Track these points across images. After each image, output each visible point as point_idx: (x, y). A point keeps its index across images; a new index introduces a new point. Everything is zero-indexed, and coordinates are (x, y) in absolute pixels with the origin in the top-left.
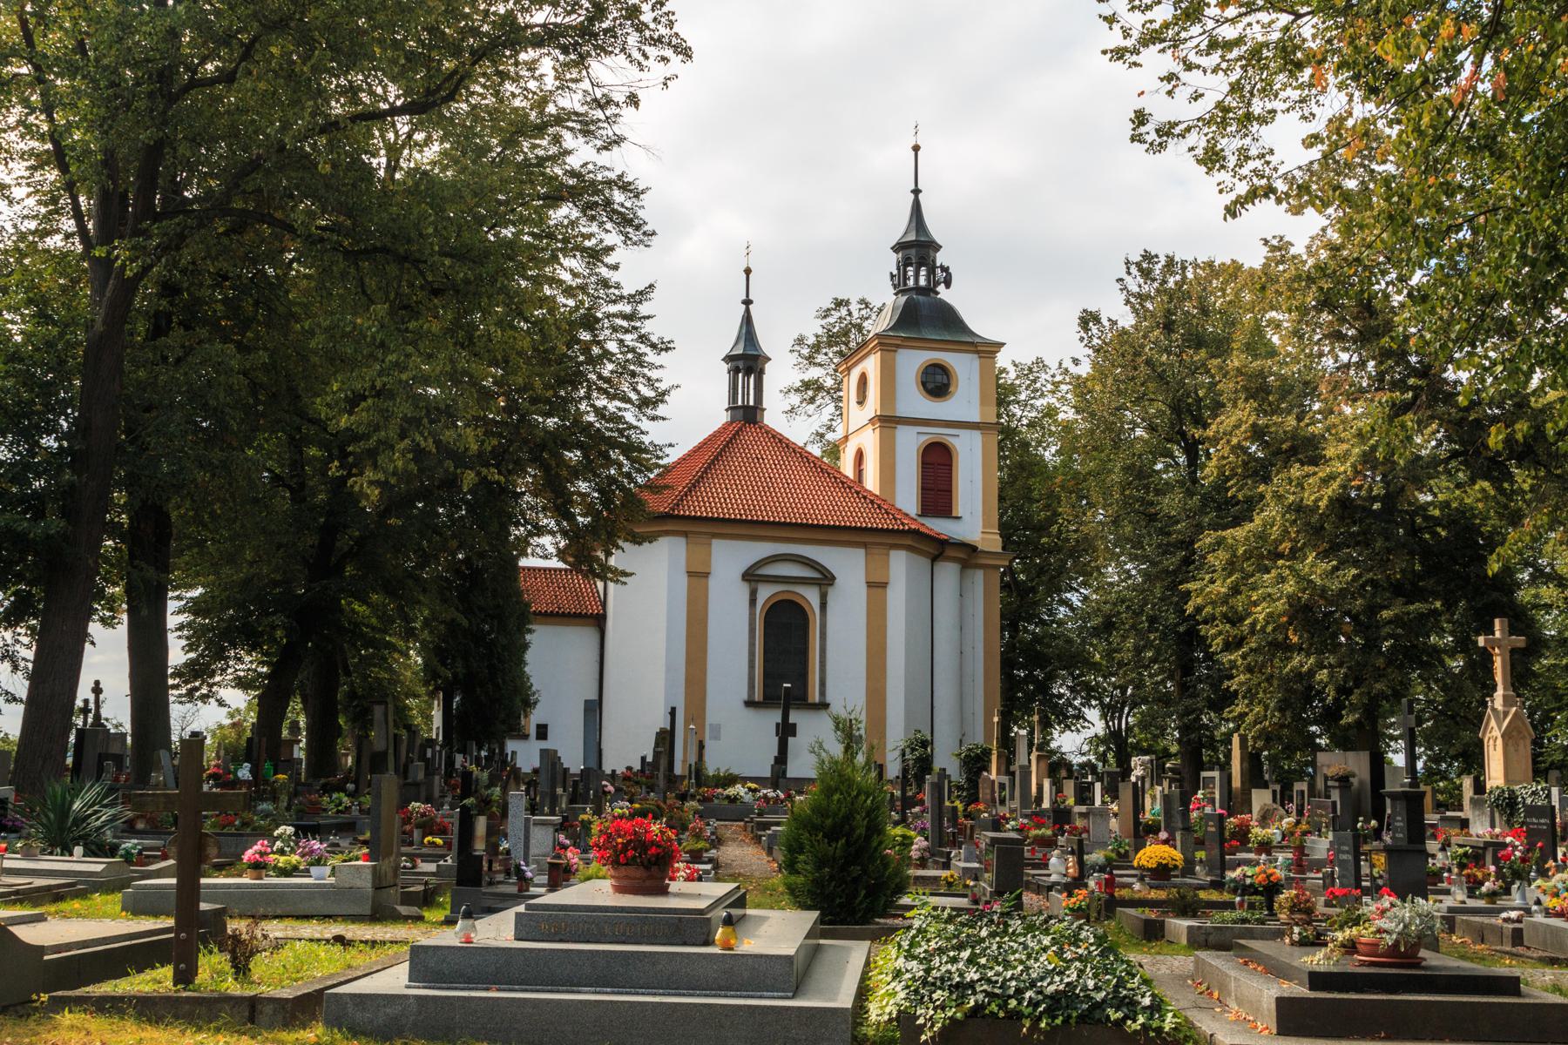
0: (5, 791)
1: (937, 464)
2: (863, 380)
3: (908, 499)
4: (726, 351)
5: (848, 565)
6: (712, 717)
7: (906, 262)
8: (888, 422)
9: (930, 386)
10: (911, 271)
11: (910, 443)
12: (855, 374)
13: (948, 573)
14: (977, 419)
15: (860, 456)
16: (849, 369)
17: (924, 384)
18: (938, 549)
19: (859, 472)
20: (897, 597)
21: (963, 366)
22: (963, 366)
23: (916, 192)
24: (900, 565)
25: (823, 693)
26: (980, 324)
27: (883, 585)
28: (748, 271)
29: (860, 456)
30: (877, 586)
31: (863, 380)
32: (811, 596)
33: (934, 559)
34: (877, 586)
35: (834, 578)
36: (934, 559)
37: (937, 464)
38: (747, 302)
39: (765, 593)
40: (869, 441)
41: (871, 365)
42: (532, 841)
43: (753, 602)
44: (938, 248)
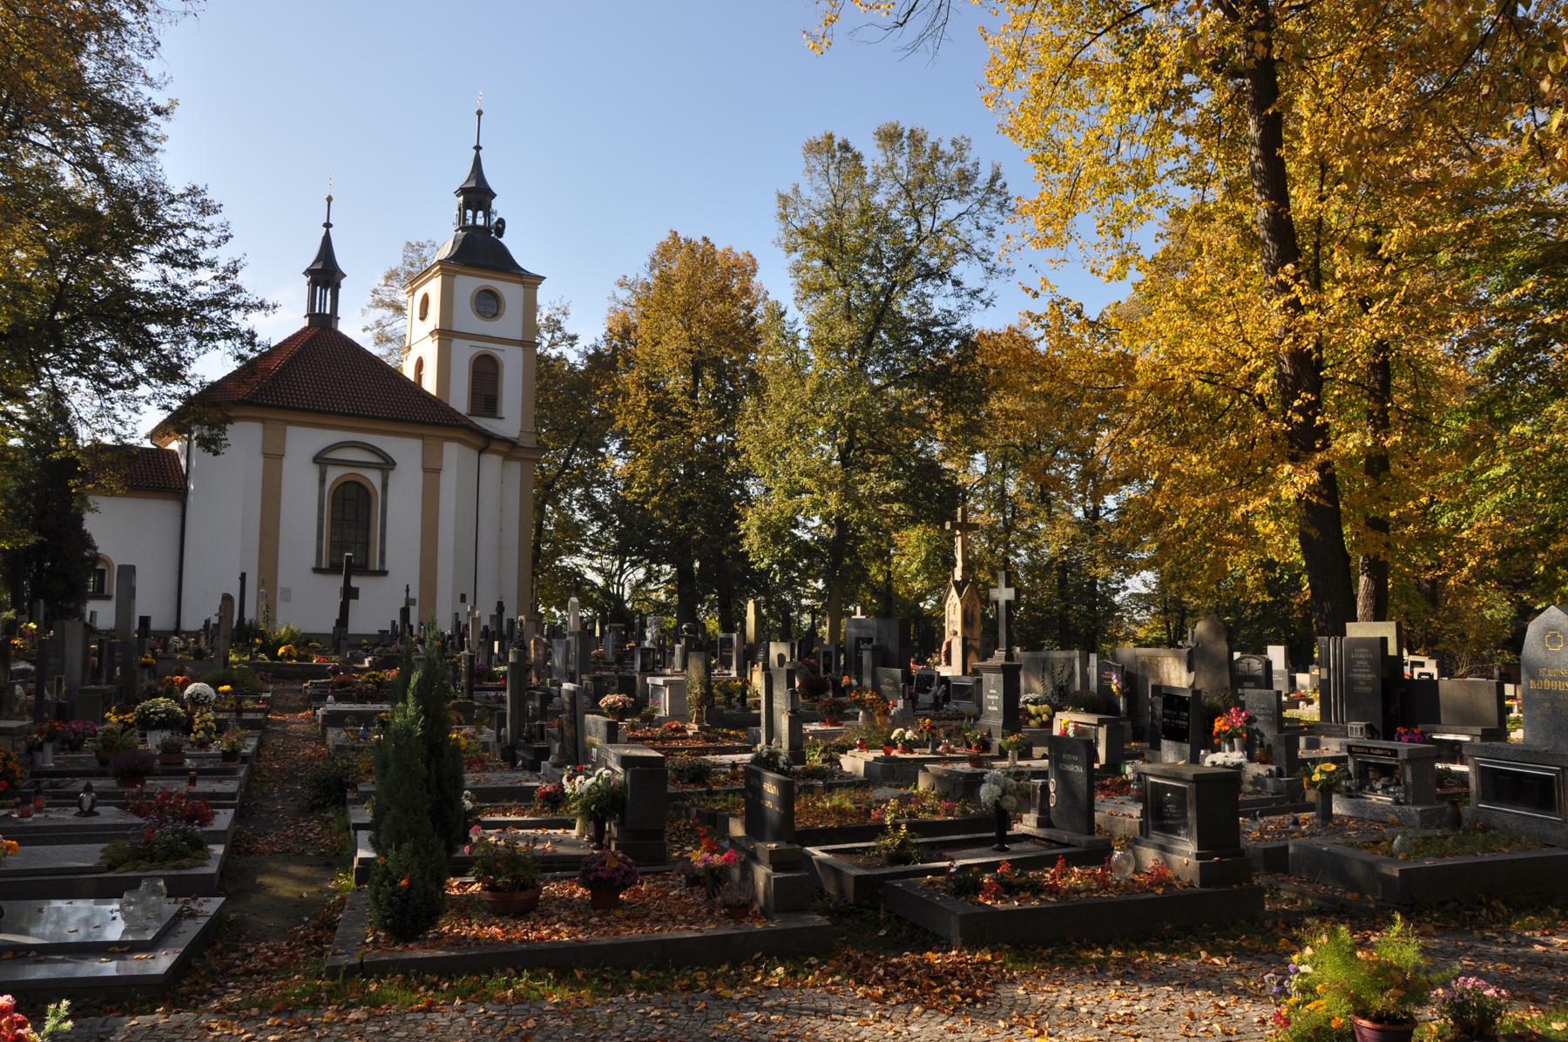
1: (485, 373)
2: (425, 301)
3: (460, 401)
5: (406, 451)
6: (283, 581)
7: (467, 205)
8: (445, 334)
11: (464, 353)
13: (492, 462)
15: (420, 364)
18: (486, 442)
20: (449, 481)
21: (509, 291)
22: (509, 291)
23: (478, 148)
24: (454, 454)
25: (382, 562)
27: (438, 471)
28: (329, 199)
29: (420, 364)
30: (432, 471)
31: (425, 301)
32: (374, 477)
33: (481, 451)
34: (432, 471)
35: (394, 464)
36: (481, 451)
37: (485, 373)
38: (478, 148)
39: (334, 474)
40: (428, 350)
41: (433, 288)
43: (322, 481)
44: (493, 195)
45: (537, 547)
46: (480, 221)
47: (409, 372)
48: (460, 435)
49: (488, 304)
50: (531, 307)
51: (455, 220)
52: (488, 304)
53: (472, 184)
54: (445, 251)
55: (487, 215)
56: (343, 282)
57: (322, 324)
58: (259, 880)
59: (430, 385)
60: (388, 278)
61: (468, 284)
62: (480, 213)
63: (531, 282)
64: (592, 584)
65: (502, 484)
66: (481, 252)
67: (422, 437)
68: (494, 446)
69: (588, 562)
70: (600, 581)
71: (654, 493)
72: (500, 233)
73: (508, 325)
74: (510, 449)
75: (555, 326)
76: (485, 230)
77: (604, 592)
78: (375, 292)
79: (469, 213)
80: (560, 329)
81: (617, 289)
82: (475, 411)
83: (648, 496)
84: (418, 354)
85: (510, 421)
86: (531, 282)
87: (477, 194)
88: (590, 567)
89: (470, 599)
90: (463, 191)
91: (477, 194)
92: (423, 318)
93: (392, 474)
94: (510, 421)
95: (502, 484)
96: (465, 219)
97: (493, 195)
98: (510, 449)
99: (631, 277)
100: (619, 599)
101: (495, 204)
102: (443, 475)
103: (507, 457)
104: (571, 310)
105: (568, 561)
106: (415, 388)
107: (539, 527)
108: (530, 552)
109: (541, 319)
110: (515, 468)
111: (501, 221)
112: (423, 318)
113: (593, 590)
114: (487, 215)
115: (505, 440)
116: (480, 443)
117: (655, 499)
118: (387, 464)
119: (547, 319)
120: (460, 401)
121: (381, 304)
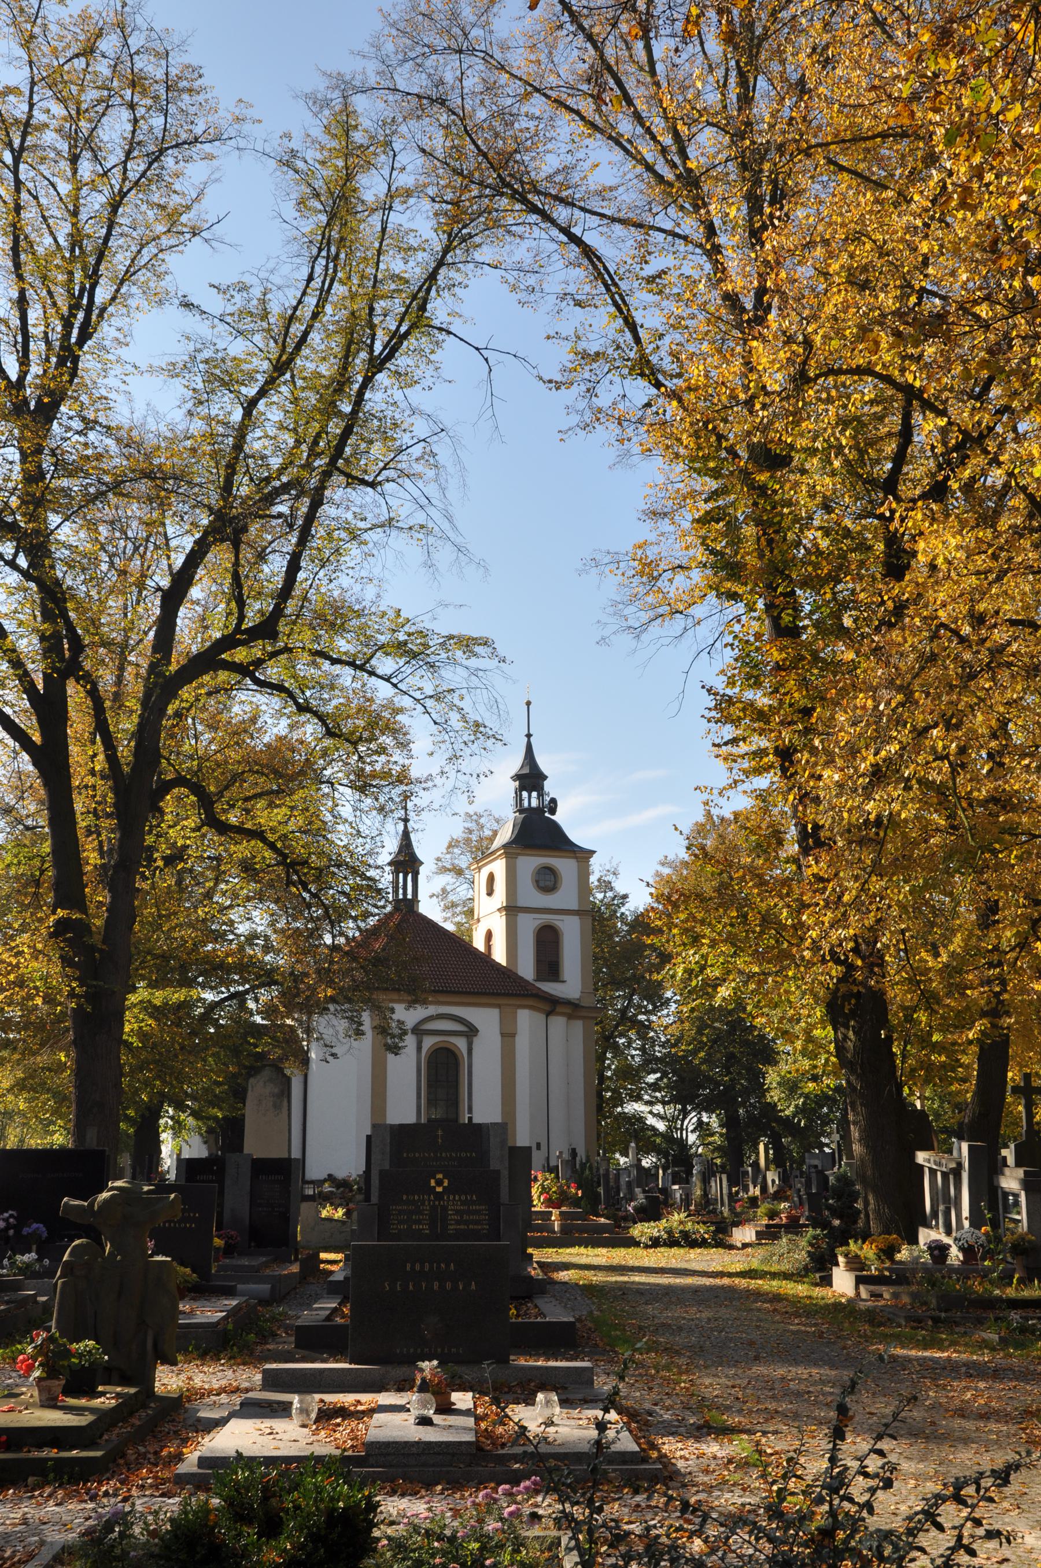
0: (862, 2)
1: (548, 942)
2: (491, 878)
3: (527, 970)
4: (513, 772)
5: (486, 1019)
7: (522, 788)
8: (511, 910)
9: (542, 884)
10: (525, 794)
11: (529, 925)
12: (485, 872)
13: (558, 1023)
14: (575, 906)
15: (489, 935)
16: (480, 868)
17: (537, 882)
18: (552, 1005)
19: (489, 947)
22: (565, 866)
23: (529, 736)
24: (526, 1019)
26: (576, 835)
27: (513, 1035)
29: (489, 935)
30: (508, 1036)
31: (491, 878)
32: (461, 1043)
33: (548, 1014)
34: (508, 1036)
36: (548, 1014)
37: (548, 942)
38: (529, 736)
39: (428, 1042)
40: (498, 925)
41: (499, 867)
42: (652, 1265)
43: (419, 1049)
44: (545, 778)
45: (600, 1097)
46: (534, 803)
47: (479, 944)
48: (530, 1002)
49: (547, 881)
50: (584, 873)
51: (513, 802)
52: (547, 881)
53: (526, 771)
54: (506, 834)
55: (541, 795)
56: (422, 869)
57: (407, 907)
58: (530, 1250)
59: (500, 955)
60: (450, 846)
61: (530, 863)
62: (534, 794)
63: (583, 855)
64: (653, 1129)
65: (567, 1038)
66: (538, 833)
67: (499, 1006)
68: (559, 1009)
69: (647, 1109)
70: (661, 1126)
71: (701, 1049)
72: (553, 811)
73: (566, 897)
74: (572, 1009)
75: (607, 886)
76: (540, 810)
77: (667, 1137)
78: (438, 859)
79: (525, 794)
80: (612, 889)
81: (660, 868)
82: (540, 977)
83: (695, 1053)
84: (490, 931)
85: (571, 984)
86: (586, 855)
87: (531, 778)
88: (651, 1112)
89: (544, 1147)
90: (517, 777)
91: (531, 778)
92: (490, 893)
93: (475, 1039)
94: (571, 984)
95: (567, 1038)
96: (521, 800)
97: (545, 778)
98: (572, 1009)
99: (671, 857)
100: (682, 1144)
101: (547, 785)
102: (517, 1038)
103: (570, 1017)
104: (620, 870)
105: (633, 1107)
106: (485, 959)
107: (602, 1078)
108: (594, 1101)
109: (593, 879)
110: (578, 1026)
111: (553, 801)
112: (490, 893)
113: (655, 1135)
114: (541, 795)
115: (568, 1003)
116: (547, 1008)
117: (702, 1054)
118: (471, 1032)
119: (599, 880)
120: (527, 970)
121: (444, 870)
